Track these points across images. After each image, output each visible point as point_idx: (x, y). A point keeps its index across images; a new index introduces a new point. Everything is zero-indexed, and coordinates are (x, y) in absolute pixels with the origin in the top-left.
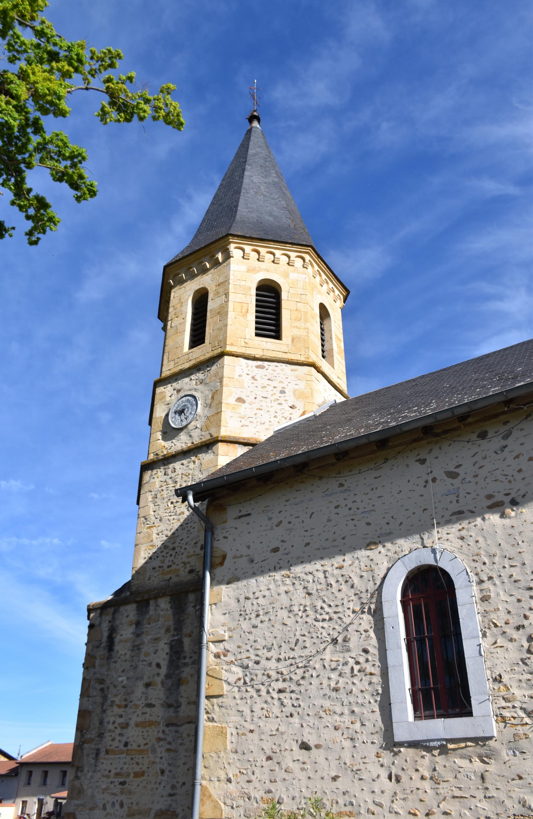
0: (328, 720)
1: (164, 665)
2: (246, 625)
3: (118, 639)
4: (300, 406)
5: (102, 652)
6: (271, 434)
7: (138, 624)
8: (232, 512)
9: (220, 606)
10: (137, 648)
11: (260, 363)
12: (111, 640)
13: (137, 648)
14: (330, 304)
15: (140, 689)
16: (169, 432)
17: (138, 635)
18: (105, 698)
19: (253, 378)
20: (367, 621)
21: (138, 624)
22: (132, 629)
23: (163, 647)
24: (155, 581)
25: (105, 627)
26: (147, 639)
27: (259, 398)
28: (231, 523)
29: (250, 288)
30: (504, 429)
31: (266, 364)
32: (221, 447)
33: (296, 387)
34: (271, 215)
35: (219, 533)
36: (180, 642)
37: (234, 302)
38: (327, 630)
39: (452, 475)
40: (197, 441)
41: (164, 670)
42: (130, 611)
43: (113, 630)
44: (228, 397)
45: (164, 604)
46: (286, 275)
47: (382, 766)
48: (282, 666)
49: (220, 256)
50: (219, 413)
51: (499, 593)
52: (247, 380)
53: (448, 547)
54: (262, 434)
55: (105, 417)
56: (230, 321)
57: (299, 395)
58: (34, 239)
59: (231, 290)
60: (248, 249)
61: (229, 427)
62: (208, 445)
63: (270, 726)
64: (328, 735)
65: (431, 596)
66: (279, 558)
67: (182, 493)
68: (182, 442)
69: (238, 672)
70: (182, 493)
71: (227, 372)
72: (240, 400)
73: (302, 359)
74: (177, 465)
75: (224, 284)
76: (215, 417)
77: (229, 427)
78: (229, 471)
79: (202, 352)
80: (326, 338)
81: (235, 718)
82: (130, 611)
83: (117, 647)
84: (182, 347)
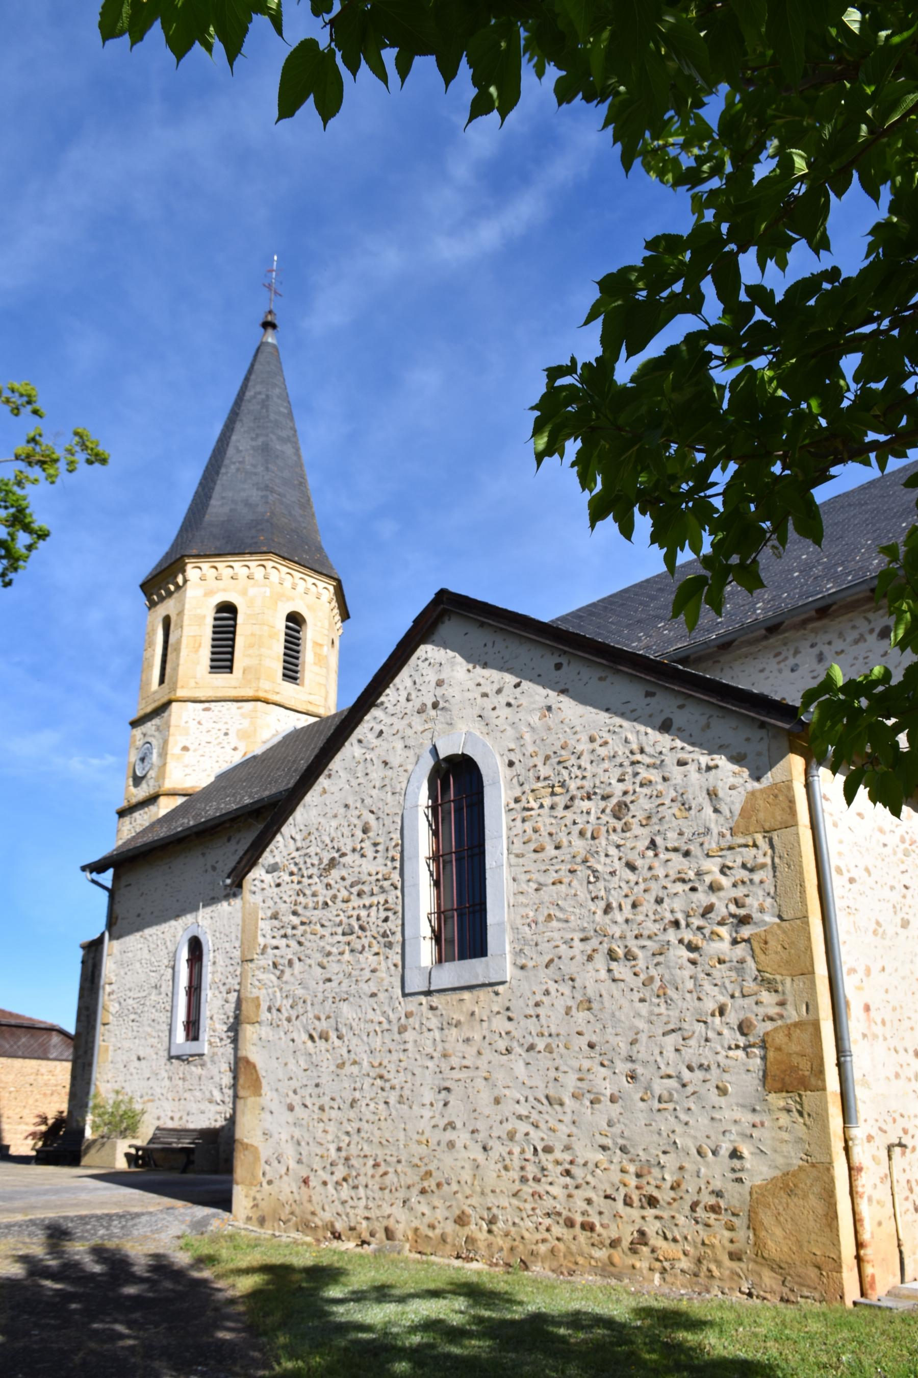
6: (212, 779)
11: (207, 705)
14: (308, 606)
19: (199, 723)
27: (203, 744)
29: (204, 617)
30: (603, 675)
31: (213, 704)
32: (163, 800)
33: (240, 727)
39: (214, 868)
44: (174, 749)
46: (244, 593)
47: (716, 985)
49: (172, 588)
50: (165, 764)
52: (193, 725)
55: (387, 528)
57: (244, 735)
58: (7, 579)
60: (205, 566)
62: (152, 799)
71: (174, 720)
72: (185, 749)
73: (249, 693)
75: (181, 613)
78: (140, 842)
84: (149, 684)
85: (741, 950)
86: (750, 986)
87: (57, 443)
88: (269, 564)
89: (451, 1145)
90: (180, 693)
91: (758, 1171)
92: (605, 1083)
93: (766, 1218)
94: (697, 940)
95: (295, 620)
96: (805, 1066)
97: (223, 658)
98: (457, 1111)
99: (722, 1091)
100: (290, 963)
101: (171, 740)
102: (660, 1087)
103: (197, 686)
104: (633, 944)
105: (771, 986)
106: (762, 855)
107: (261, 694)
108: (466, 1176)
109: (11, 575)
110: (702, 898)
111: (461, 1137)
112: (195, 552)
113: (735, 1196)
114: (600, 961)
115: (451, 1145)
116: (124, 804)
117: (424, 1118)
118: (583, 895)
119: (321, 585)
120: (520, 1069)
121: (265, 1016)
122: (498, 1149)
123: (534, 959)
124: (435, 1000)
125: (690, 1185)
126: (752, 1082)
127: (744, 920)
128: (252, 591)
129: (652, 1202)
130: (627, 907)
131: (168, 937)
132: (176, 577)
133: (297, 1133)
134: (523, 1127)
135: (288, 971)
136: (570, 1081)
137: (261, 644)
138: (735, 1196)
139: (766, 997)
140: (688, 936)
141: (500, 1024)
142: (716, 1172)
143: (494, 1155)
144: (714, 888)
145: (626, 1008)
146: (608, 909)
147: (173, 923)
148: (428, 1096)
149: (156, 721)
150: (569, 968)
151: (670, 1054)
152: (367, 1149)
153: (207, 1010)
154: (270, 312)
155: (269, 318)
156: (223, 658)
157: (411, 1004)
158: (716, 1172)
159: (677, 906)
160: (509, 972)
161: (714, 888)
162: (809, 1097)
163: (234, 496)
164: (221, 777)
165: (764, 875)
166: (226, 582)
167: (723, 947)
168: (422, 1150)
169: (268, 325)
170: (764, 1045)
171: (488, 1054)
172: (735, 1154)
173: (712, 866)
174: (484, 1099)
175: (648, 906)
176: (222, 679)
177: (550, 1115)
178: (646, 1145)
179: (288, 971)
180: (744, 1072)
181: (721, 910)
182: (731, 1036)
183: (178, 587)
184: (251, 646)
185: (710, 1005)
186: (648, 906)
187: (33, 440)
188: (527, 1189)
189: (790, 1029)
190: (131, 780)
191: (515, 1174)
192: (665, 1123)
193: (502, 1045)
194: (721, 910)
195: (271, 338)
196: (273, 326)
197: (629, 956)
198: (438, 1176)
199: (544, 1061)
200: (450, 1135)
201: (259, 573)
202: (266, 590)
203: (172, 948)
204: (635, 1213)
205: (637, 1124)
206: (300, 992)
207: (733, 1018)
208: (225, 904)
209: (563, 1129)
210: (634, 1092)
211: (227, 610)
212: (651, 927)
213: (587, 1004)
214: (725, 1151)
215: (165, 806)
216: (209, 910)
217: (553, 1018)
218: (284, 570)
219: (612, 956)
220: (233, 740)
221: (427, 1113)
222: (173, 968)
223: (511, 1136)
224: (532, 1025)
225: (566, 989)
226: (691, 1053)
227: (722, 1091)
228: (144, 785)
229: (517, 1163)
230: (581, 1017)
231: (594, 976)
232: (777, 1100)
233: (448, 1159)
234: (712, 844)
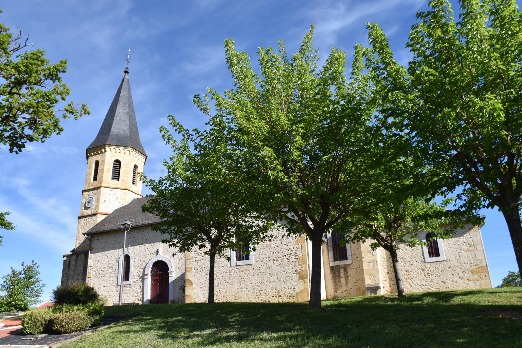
0: (109, 282)
1: (82, 270)
2: (96, 263)
5: (67, 267)
6: (113, 211)
7: (76, 260)
8: (95, 239)
9: (92, 258)
12: (69, 264)
13: (76, 266)
15: (76, 276)
16: (86, 208)
17: (76, 263)
20: (117, 263)
21: (76, 260)
24: (81, 250)
26: (78, 264)
28: (95, 241)
34: (123, 130)
35: (93, 243)
38: (110, 265)
39: (134, 237)
40: (93, 213)
41: (82, 272)
42: (74, 257)
43: (70, 262)
44: (102, 200)
46: (123, 158)
48: (102, 272)
49: (103, 150)
50: (99, 205)
51: (136, 260)
53: (131, 251)
54: (110, 211)
56: (104, 175)
57: (122, 199)
59: (105, 164)
60: (112, 148)
61: (101, 209)
62: (95, 215)
63: (99, 283)
64: (108, 284)
65: (127, 258)
66: (103, 249)
67: (84, 234)
68: (88, 212)
69: (94, 273)
70: (84, 234)
72: (105, 201)
73: (124, 187)
74: (87, 218)
75: (103, 161)
76: (97, 206)
77: (101, 209)
79: (96, 184)
81: (93, 282)
82: (74, 257)
83: (71, 266)
84: (90, 180)
85: (296, 260)
86: (297, 265)
87: (77, 108)
88: (131, 150)
89: (242, 291)
90: (103, 185)
91: (297, 290)
92: (272, 280)
93: (299, 296)
94: (289, 258)
95: (136, 167)
96: (305, 276)
97: (116, 176)
98: (243, 285)
99: (292, 280)
100: (200, 260)
101: (101, 198)
102: (282, 280)
103: (108, 183)
104: (278, 259)
105: (300, 265)
106: (300, 246)
107: (127, 188)
108: (245, 296)
109: (44, 139)
110: (290, 252)
111: (244, 290)
112: (109, 143)
113: (294, 294)
114: (272, 261)
115: (242, 291)
116: (81, 215)
117: (235, 287)
118: (269, 250)
119: (142, 157)
120: (256, 278)
121: (193, 270)
122: (251, 291)
123: (258, 260)
124: (238, 267)
125: (287, 293)
126: (297, 278)
127: (296, 256)
128: (125, 158)
129: (280, 296)
130: (277, 253)
131: (115, 254)
132: (101, 149)
133: (203, 292)
134: (257, 287)
135: (199, 262)
136: (266, 280)
137: (126, 172)
138: (294, 294)
139: (299, 266)
140: (287, 257)
141: (252, 271)
142: (291, 291)
143: (251, 292)
144: (292, 251)
145: (276, 268)
146: (273, 253)
147: (117, 250)
148: (236, 283)
149: (94, 192)
150: (265, 262)
151: (284, 275)
152: (222, 294)
153: (425, 253)
154: (127, 68)
155: (127, 70)
156: (116, 176)
157: (232, 268)
158: (291, 291)
159: (286, 253)
160: (254, 262)
161: (292, 251)
162: (305, 280)
163: (120, 126)
164: (116, 211)
165: (300, 249)
166: (118, 154)
167: (293, 259)
168: (235, 293)
169: (126, 72)
170: (299, 273)
171: (249, 276)
172: (294, 288)
173: (292, 247)
174: (249, 283)
175: (281, 253)
176: (115, 182)
177: (262, 285)
178: (279, 288)
179: (199, 262)
180: (296, 277)
181: (293, 254)
182: (294, 272)
183: (102, 152)
184: (125, 174)
185: (291, 268)
186: (281, 253)
187: (70, 105)
188: (257, 297)
189: (303, 271)
190: (83, 208)
191: (255, 295)
192: (283, 285)
193: (252, 274)
194: (293, 254)
195: (127, 77)
196: (128, 72)
197: (277, 260)
198: (238, 297)
199: (261, 276)
200: (241, 289)
201: (128, 152)
202: (129, 158)
203: (117, 257)
204: (277, 298)
205: (278, 286)
206: (203, 266)
207: (294, 269)
208: (138, 246)
209: (264, 287)
210: (277, 281)
211: (118, 163)
212: (281, 256)
213: (269, 268)
214: (293, 288)
215: (100, 218)
216: (132, 247)
217: (262, 269)
218: (134, 152)
219: (274, 260)
220: (119, 200)
221: (236, 286)
222: (118, 263)
223: (254, 289)
224: (258, 271)
225: (265, 265)
226: (287, 275)
227: (292, 280)
228: (89, 210)
229: (255, 293)
230: (268, 270)
231: (270, 263)
232: (301, 281)
233: (241, 294)
234: (292, 244)
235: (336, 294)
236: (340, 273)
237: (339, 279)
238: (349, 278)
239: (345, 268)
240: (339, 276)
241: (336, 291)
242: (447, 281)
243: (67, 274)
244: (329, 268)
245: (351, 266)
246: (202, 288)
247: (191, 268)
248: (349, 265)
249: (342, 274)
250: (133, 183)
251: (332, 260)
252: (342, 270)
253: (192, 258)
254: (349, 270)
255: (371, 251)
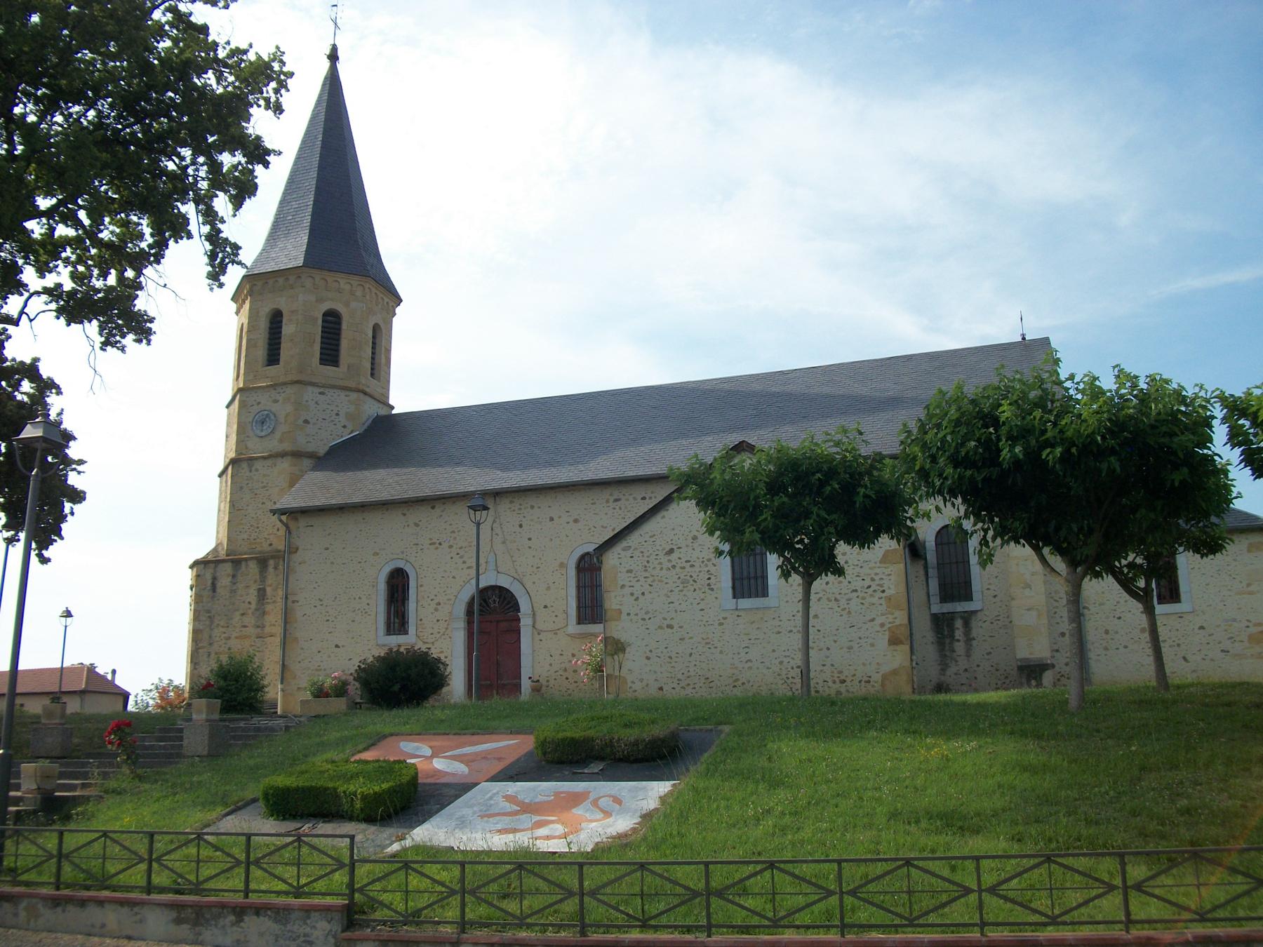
3: (219, 585)
4: (350, 428)
10: (233, 591)
15: (237, 615)
18: (212, 622)
21: (234, 576)
22: (230, 579)
23: (253, 593)
24: (222, 554)
25: (209, 576)
36: (264, 590)
37: (352, 838)
39: (417, 525)
41: (253, 606)
42: (228, 568)
45: (253, 566)
46: (347, 304)
57: (350, 417)
73: (352, 384)
80: (377, 361)
83: (218, 590)
88: (367, 286)
107: (361, 387)
134: (786, 660)
176: (329, 370)
200: (749, 664)
223: (781, 663)
235: (943, 678)
236: (953, 631)
237: (951, 643)
238: (974, 643)
239: (968, 617)
240: (952, 636)
241: (943, 670)
242: (265, 827)
243: (209, 611)
244: (928, 617)
245: (979, 615)
246: (648, 658)
247: (620, 612)
248: (974, 612)
249: (959, 634)
250: (372, 375)
251: (935, 599)
252: (959, 623)
253: (623, 586)
254: (974, 623)
255: (98, 345)
